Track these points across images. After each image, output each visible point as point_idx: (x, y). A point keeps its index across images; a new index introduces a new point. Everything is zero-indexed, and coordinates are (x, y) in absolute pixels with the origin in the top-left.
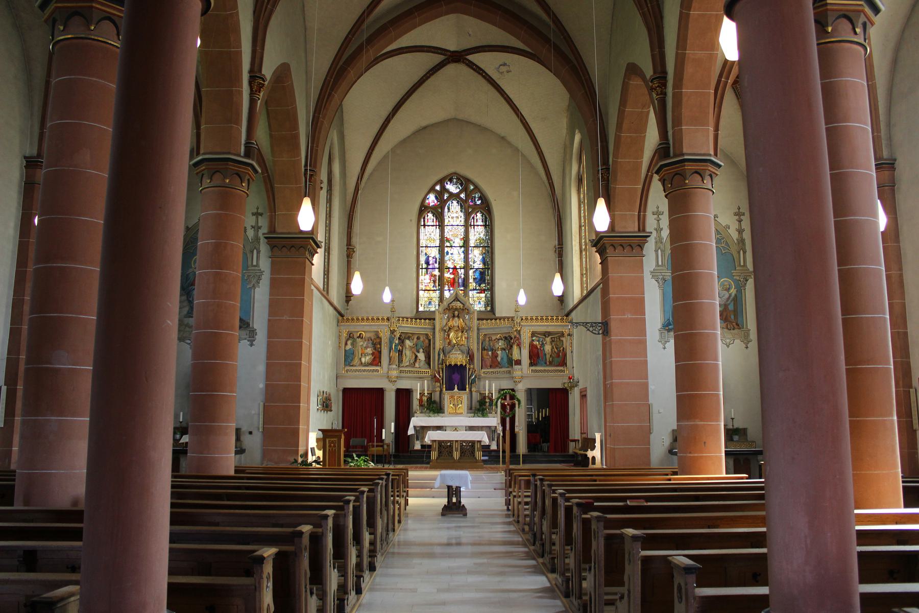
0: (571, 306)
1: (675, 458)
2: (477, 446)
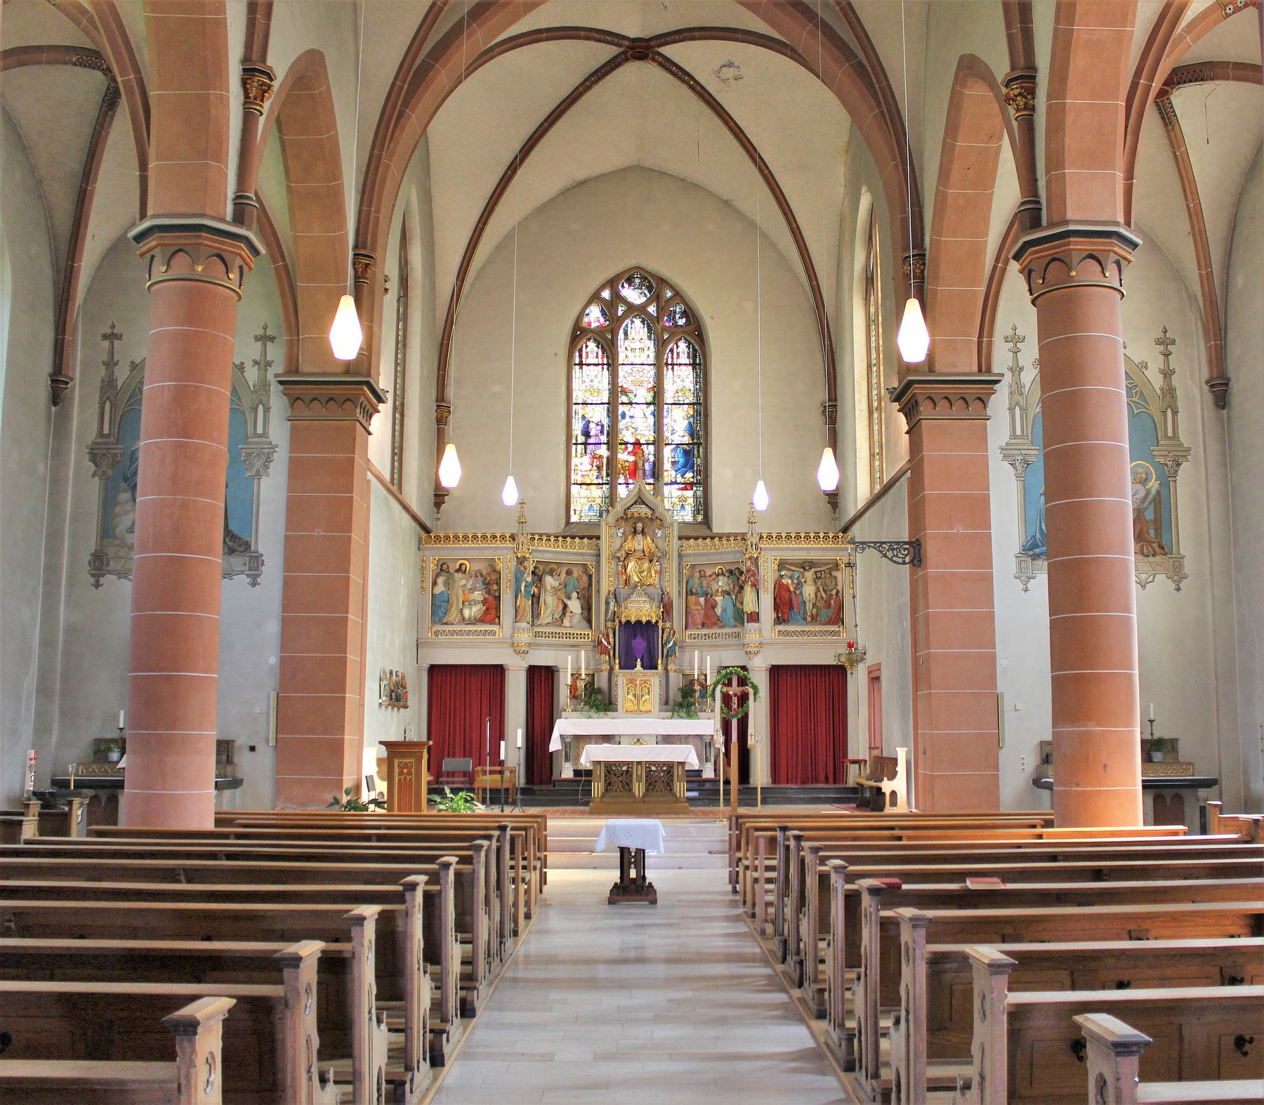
0: (851, 513)
1: (1046, 793)
2: (677, 772)
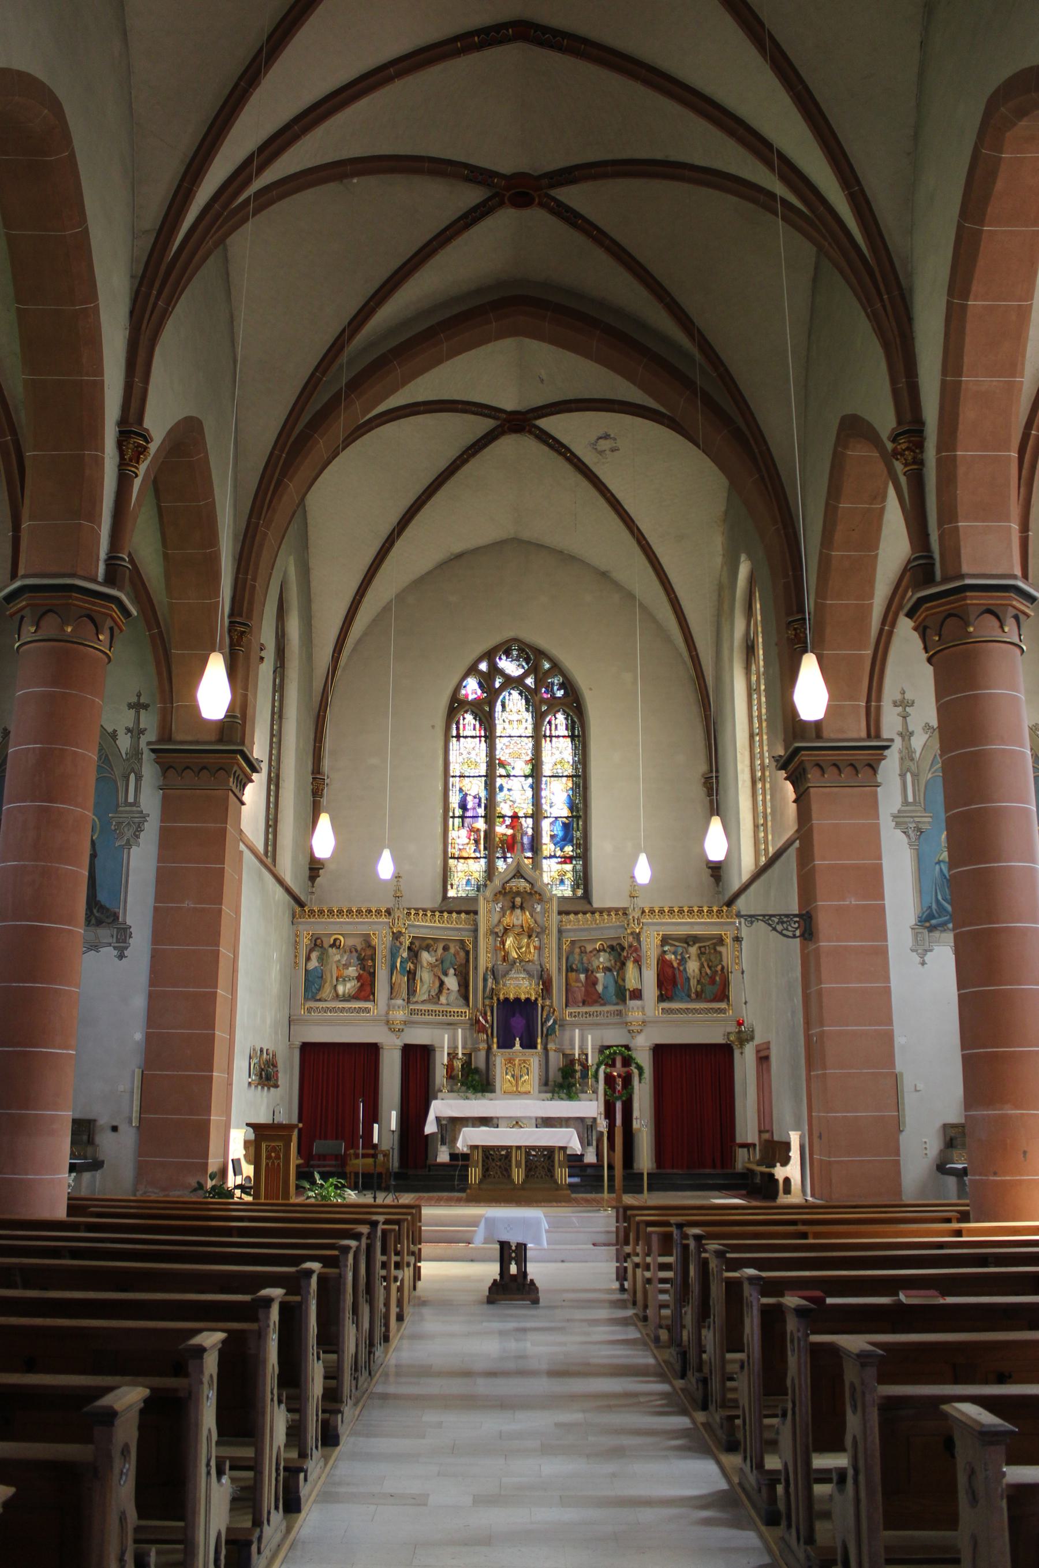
0: (736, 886)
2: (559, 1157)
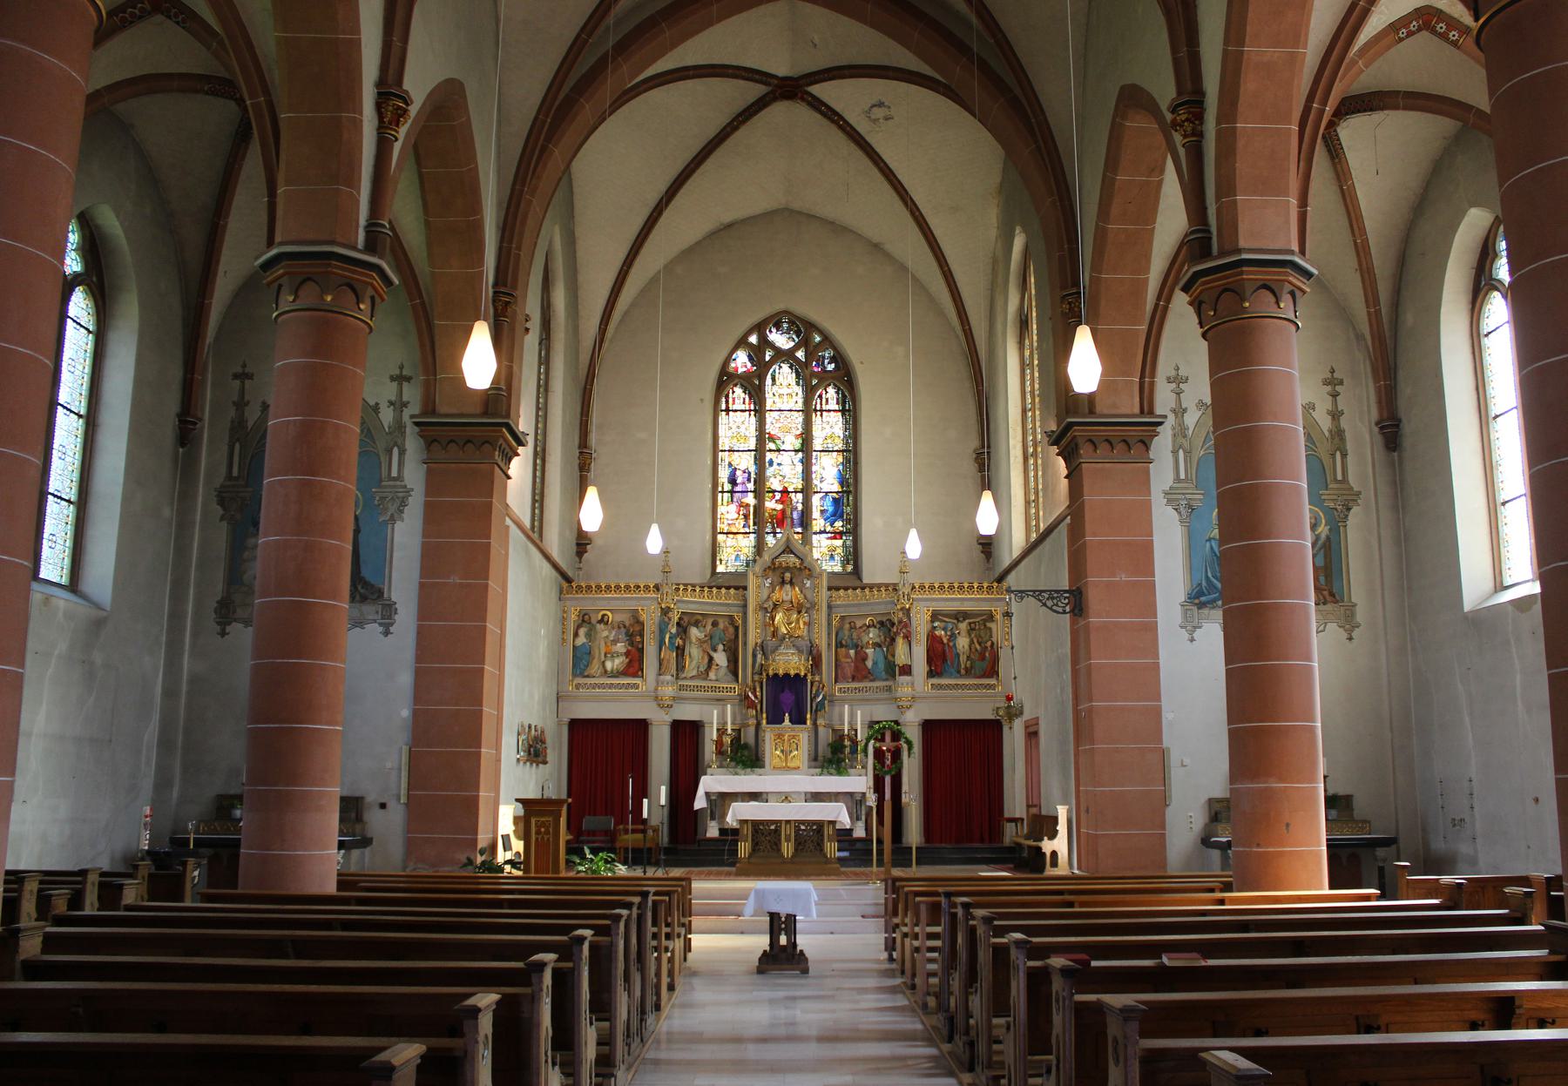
0: (1006, 562)
